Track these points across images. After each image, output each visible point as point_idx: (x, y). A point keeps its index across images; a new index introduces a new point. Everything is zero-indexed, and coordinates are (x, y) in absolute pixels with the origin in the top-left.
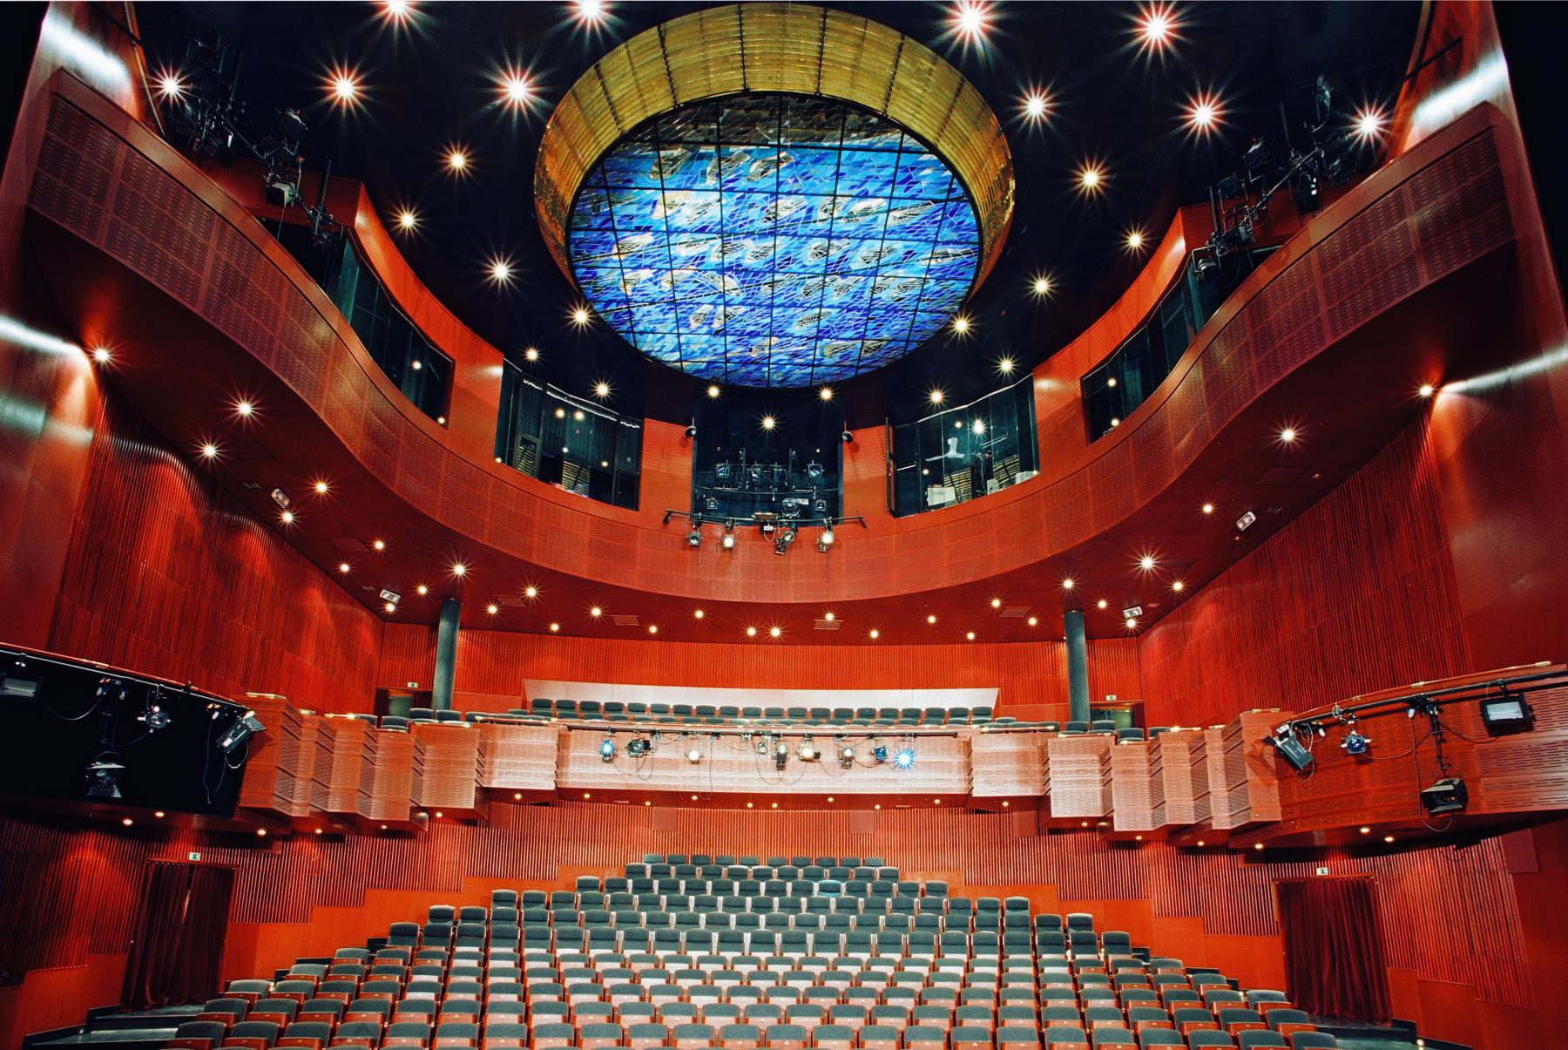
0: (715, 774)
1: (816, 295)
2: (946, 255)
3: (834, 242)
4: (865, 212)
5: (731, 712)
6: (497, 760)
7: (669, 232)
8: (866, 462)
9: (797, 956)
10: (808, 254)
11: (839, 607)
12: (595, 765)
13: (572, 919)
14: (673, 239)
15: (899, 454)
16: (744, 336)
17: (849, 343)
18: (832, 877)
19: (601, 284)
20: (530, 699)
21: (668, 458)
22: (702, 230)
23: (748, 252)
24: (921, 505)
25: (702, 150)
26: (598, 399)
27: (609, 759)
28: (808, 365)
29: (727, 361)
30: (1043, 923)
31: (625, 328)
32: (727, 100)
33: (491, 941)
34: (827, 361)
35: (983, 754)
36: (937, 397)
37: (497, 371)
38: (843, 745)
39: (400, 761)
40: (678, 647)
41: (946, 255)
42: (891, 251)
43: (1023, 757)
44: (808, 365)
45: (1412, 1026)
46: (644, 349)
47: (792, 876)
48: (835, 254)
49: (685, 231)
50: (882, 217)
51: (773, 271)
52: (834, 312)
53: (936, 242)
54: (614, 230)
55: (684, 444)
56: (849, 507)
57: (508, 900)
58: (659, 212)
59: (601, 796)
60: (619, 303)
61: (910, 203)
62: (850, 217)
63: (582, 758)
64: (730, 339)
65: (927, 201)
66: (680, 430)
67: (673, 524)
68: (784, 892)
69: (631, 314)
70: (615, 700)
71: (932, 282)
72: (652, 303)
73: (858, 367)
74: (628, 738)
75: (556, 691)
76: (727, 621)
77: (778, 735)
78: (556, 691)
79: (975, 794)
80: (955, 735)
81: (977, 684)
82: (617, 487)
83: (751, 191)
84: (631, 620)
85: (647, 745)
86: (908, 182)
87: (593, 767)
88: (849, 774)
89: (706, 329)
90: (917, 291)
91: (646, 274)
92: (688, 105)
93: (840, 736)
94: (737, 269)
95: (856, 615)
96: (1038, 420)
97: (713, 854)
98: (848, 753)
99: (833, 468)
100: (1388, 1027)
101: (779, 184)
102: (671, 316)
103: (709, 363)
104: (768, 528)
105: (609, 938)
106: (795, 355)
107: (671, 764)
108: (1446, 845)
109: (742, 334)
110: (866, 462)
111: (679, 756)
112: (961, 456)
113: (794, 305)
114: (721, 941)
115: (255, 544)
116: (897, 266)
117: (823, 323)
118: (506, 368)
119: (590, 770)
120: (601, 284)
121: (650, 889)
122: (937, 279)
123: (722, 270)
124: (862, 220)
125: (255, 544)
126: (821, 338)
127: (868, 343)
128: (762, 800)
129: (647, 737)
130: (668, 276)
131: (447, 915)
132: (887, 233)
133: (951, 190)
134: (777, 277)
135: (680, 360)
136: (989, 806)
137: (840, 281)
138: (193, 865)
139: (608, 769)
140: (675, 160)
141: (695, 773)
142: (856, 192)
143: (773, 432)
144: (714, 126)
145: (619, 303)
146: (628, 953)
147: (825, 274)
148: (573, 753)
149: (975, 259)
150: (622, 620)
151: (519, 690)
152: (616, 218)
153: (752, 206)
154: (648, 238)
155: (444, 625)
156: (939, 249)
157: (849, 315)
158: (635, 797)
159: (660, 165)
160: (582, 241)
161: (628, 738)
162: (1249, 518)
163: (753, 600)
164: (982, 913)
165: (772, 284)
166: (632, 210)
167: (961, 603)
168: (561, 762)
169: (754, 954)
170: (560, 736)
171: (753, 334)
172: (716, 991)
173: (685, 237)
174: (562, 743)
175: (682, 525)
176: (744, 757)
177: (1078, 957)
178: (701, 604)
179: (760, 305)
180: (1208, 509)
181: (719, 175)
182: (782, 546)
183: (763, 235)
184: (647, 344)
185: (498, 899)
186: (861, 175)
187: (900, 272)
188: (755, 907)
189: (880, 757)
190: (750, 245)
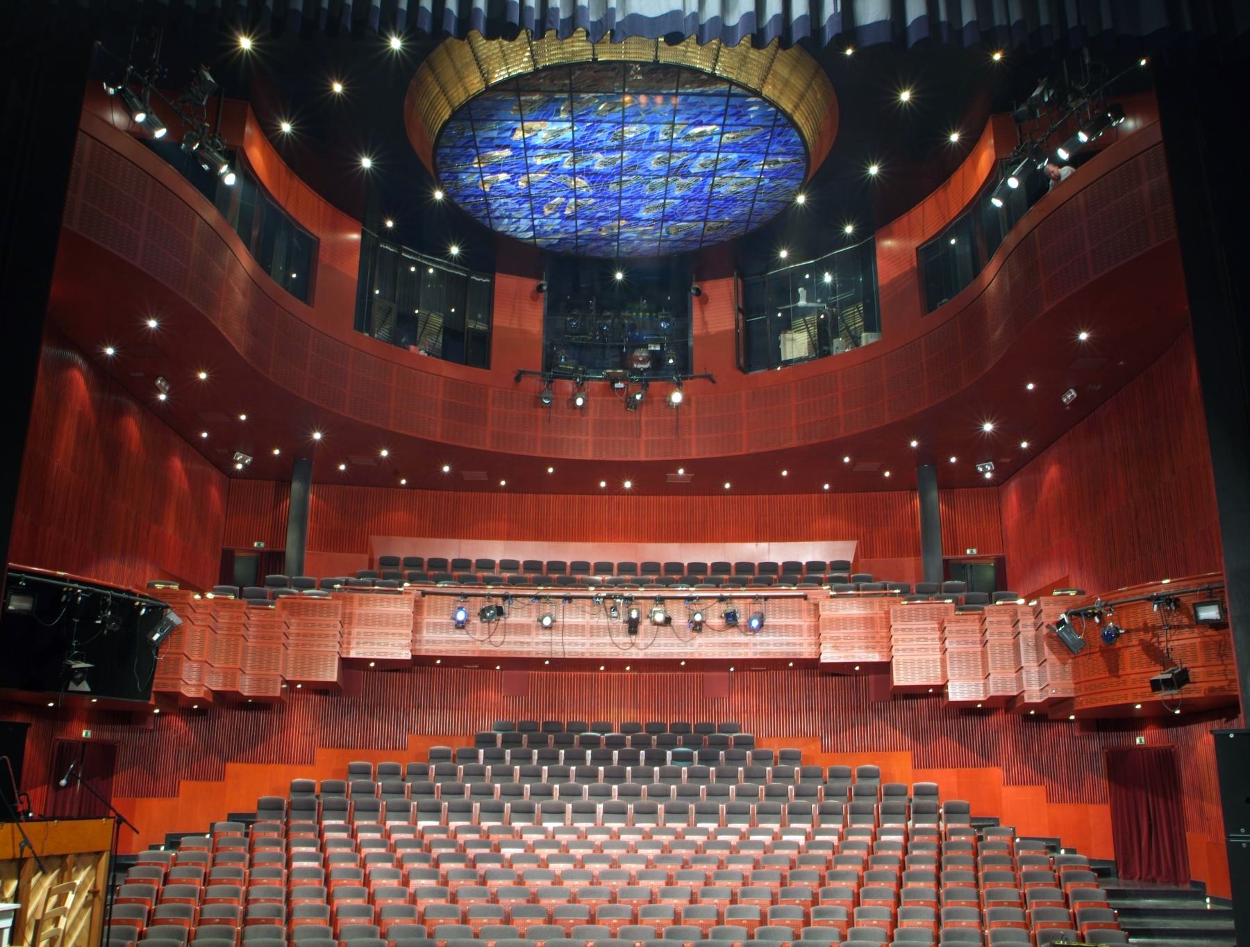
0: (567, 639)
1: (661, 191)
2: (777, 162)
3: (676, 155)
4: (701, 134)
5: (581, 567)
6: (355, 631)
7: (527, 148)
8: (716, 313)
9: (647, 826)
10: (652, 163)
11: (689, 464)
12: (448, 631)
13: (430, 791)
14: (530, 153)
15: (747, 307)
16: (591, 220)
17: (692, 224)
18: (685, 745)
19: (461, 183)
20: (377, 556)
21: (520, 314)
22: (556, 147)
23: (598, 161)
24: (773, 356)
25: (557, 96)
26: (451, 258)
27: (461, 626)
28: (655, 240)
29: (578, 237)
30: (890, 793)
31: (481, 214)
32: (581, 65)
33: (293, 813)
34: (672, 237)
35: (831, 620)
36: (784, 254)
37: (356, 236)
38: (695, 608)
39: (271, 638)
40: (529, 498)
41: (777, 162)
42: (726, 160)
43: (869, 622)
44: (655, 240)
45: (1203, 885)
46: (500, 229)
47: (644, 743)
48: (676, 162)
49: (541, 147)
50: (716, 138)
51: (621, 174)
52: (677, 202)
53: (767, 154)
54: (476, 147)
55: (534, 298)
56: (697, 366)
57: (365, 772)
58: (518, 135)
59: (451, 662)
60: (476, 197)
61: (741, 128)
62: (687, 138)
63: (435, 624)
64: (580, 222)
65: (755, 127)
66: (530, 284)
67: (524, 380)
68: (637, 760)
69: (488, 205)
70: (463, 557)
71: (767, 181)
72: (509, 196)
73: (702, 242)
74: (479, 604)
75: (404, 548)
76: (579, 476)
77: (630, 599)
78: (404, 548)
79: (824, 659)
80: (805, 597)
81: (834, 536)
82: (468, 346)
83: (600, 121)
84: (481, 475)
85: (500, 612)
86: (738, 115)
87: (448, 632)
88: (700, 639)
89: (558, 215)
90: (753, 186)
91: (503, 176)
92: (546, 68)
93: (690, 599)
94: (587, 173)
95: (707, 474)
96: (880, 283)
97: (565, 719)
98: (698, 618)
99: (682, 313)
100: (1187, 887)
101: (624, 117)
102: (527, 205)
103: (560, 239)
104: (619, 385)
105: (466, 810)
106: (644, 233)
107: (522, 629)
108: (1220, 718)
109: (592, 218)
110: (716, 313)
111: (531, 620)
112: (811, 305)
113: (641, 197)
114: (575, 811)
115: (132, 426)
116: (733, 169)
117: (668, 209)
118: (363, 234)
119: (443, 636)
120: (461, 183)
121: (502, 758)
122: (771, 179)
123: (573, 174)
124: (699, 140)
125: (132, 426)
126: (667, 221)
127: (710, 224)
128: (615, 665)
129: (500, 602)
130: (524, 178)
131: (309, 789)
132: (721, 148)
133: (776, 120)
134: (624, 178)
135: (534, 237)
136: (841, 670)
137: (681, 181)
138: (85, 742)
139: (460, 635)
140: (534, 102)
141: (547, 638)
142: (691, 121)
143: (621, 282)
144: (567, 82)
145: (476, 197)
146: (485, 825)
147: (667, 176)
148: (428, 619)
149: (804, 165)
150: (469, 475)
151: (365, 548)
152: (478, 140)
153: (600, 131)
154: (507, 152)
155: (296, 486)
156: (770, 158)
157: (691, 204)
158: (485, 663)
159: (520, 106)
160: (447, 155)
161: (479, 604)
162: (1071, 395)
163: (605, 457)
164: (859, 782)
165: (620, 183)
166: (495, 134)
167: (812, 463)
168: (416, 629)
169: (607, 825)
170: (416, 601)
171: (601, 219)
172: (571, 859)
173: (541, 152)
174: (418, 607)
175: (533, 384)
176: (595, 621)
177: (917, 826)
178: (551, 462)
179: (609, 198)
180: (953, 460)
181: (571, 112)
182: (630, 403)
183: (611, 150)
184: (504, 226)
185: (354, 772)
186: (695, 111)
187: (737, 174)
188: (608, 776)
189: (731, 619)
190: (599, 156)
